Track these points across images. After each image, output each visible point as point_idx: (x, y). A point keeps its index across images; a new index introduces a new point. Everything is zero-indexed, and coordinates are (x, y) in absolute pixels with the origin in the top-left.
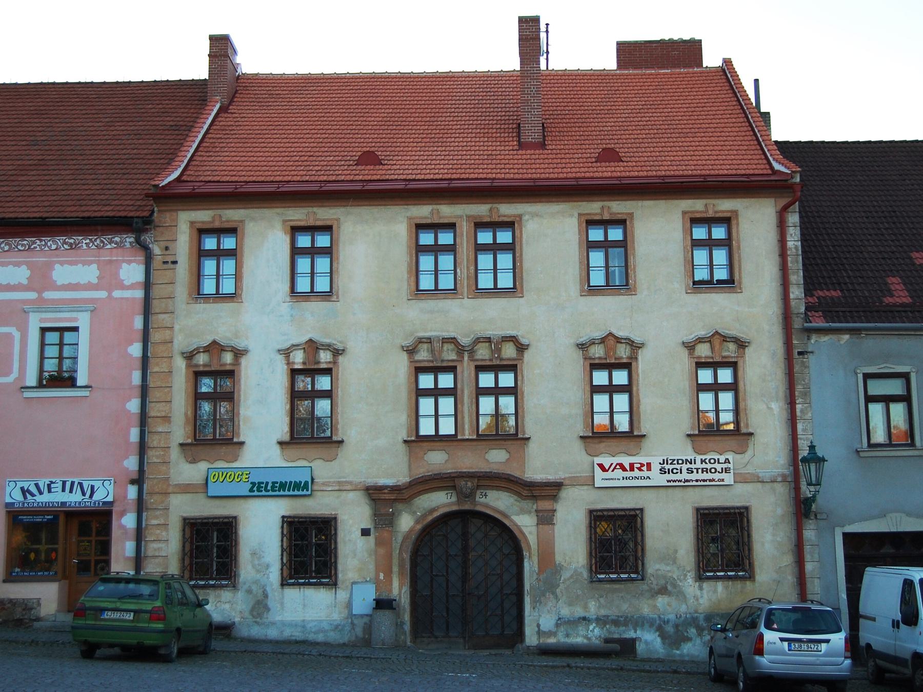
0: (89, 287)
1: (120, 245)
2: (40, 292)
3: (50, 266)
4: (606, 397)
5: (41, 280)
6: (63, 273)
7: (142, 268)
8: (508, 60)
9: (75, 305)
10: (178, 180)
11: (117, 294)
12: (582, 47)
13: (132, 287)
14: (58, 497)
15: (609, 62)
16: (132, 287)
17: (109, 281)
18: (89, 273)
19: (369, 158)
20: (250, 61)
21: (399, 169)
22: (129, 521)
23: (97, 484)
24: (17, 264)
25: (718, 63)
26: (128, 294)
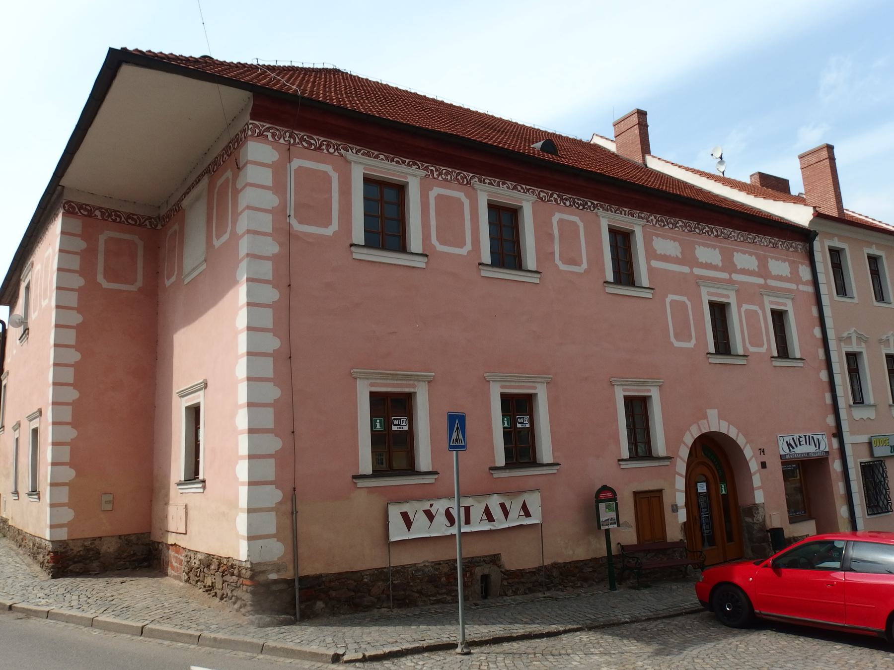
20: (254, 562)
23: (820, 437)
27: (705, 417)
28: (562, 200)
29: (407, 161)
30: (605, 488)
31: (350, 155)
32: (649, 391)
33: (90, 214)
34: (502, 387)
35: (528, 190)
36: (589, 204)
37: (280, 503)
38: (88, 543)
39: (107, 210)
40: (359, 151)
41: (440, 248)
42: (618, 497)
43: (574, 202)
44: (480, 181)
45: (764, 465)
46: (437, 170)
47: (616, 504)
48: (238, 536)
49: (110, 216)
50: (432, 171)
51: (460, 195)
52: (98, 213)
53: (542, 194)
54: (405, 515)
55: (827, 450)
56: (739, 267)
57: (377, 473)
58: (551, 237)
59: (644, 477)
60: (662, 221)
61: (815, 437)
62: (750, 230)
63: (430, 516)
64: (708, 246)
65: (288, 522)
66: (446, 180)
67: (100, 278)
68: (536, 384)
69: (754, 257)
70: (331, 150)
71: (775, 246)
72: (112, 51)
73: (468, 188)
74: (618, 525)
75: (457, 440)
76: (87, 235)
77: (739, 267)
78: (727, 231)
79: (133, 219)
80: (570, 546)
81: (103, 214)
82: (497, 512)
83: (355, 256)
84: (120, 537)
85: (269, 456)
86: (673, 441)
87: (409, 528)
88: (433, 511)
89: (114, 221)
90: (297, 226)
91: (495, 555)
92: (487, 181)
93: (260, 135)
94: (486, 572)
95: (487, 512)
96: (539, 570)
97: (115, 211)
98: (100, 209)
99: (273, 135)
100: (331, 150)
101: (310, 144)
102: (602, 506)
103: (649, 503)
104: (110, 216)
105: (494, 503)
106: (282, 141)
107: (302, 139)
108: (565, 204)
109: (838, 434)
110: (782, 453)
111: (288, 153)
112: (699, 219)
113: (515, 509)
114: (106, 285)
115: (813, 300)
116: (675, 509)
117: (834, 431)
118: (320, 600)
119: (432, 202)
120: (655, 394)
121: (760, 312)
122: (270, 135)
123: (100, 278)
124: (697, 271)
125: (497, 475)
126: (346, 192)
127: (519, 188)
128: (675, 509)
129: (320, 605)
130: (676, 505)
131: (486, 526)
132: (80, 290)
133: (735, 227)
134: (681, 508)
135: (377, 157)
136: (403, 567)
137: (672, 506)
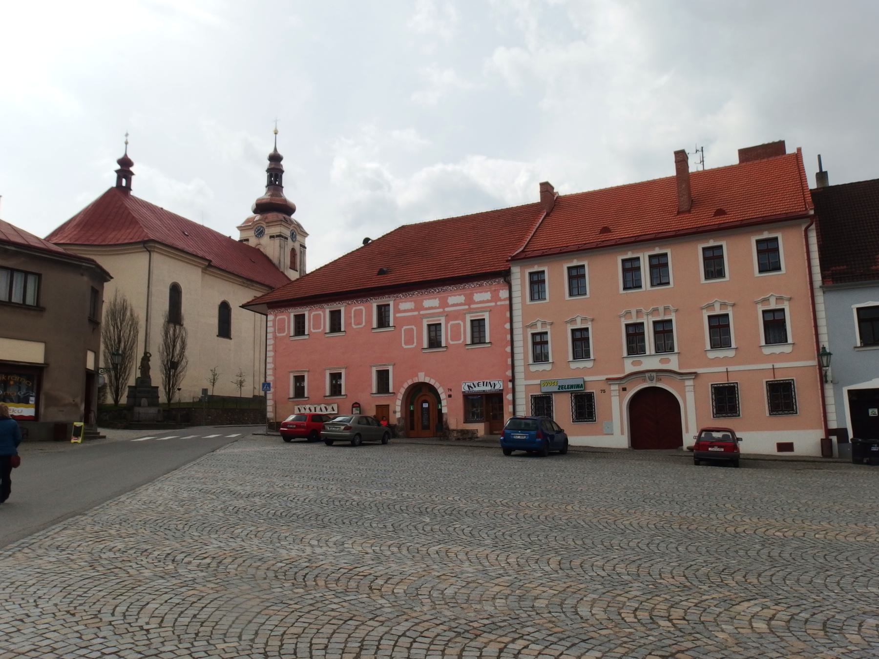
0: (488, 301)
1: (499, 283)
2: (469, 305)
3: (472, 295)
4: (14, 300)
5: (469, 301)
6: (477, 297)
7: (508, 292)
8: (671, 172)
9: (483, 310)
10: (523, 251)
11: (499, 303)
12: (722, 155)
13: (505, 300)
14: (482, 388)
15: (735, 160)
16: (505, 300)
17: (495, 298)
18: (487, 296)
19: (605, 230)
20: (563, 189)
21: (618, 234)
22: (509, 397)
23: (496, 382)
24: (460, 295)
25: (795, 151)
26: (503, 303)
27: (417, 376)
31: (291, 310)
45: (450, 396)
48: (496, 305)
51: (320, 312)
57: (473, 343)
59: (383, 400)
62: (461, 283)
82: (324, 409)
86: (397, 387)
87: (243, 306)
103: (383, 410)
105: (323, 406)
109: (513, 380)
111: (276, 316)
113: (330, 409)
116: (395, 412)
120: (390, 369)
124: (422, 312)
128: (395, 412)
133: (450, 285)
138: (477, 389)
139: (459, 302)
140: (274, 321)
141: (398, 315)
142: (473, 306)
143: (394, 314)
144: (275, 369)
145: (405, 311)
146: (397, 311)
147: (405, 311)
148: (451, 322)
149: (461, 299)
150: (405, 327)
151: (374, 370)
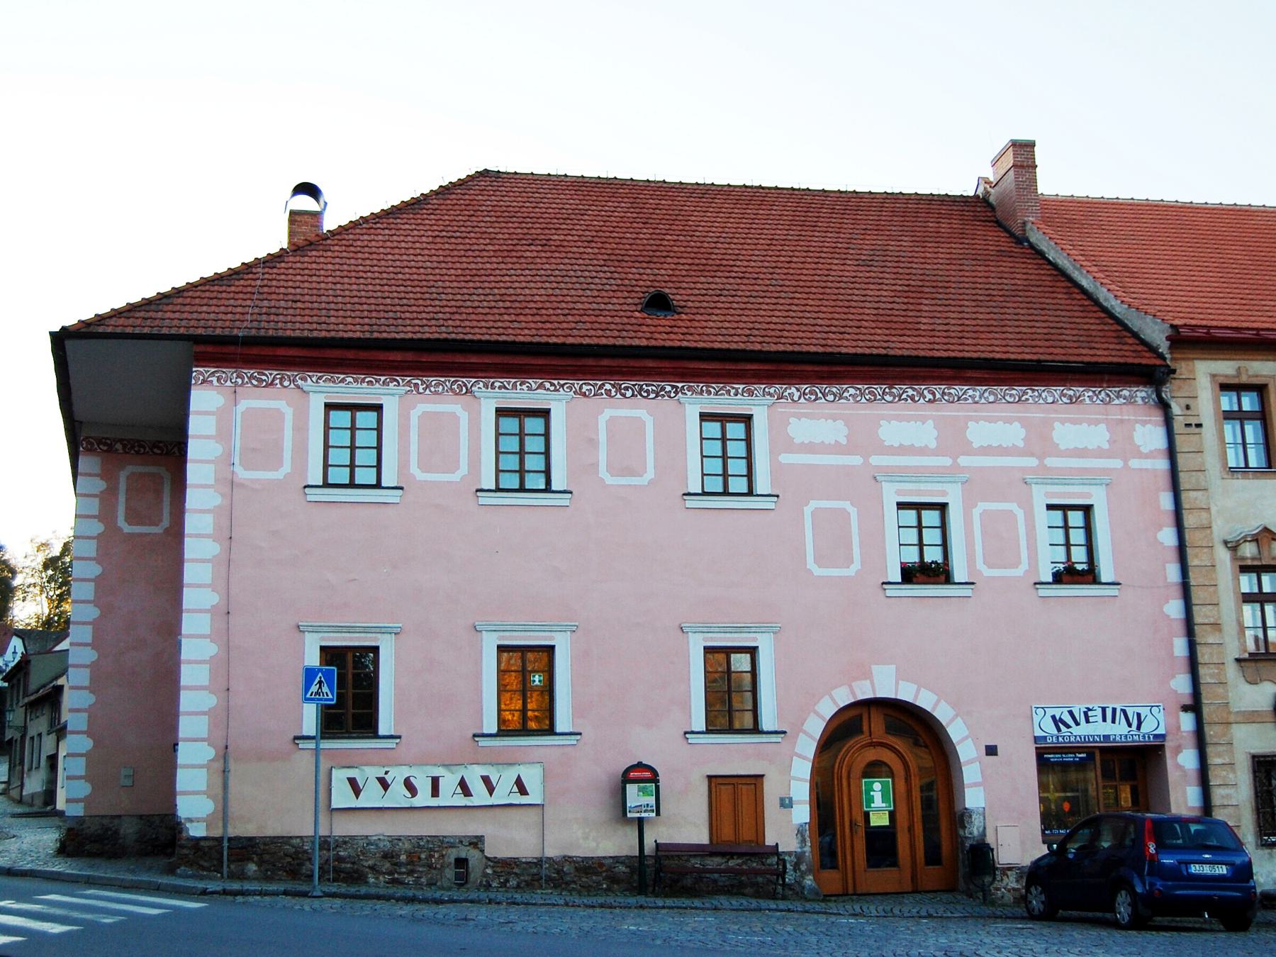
0: (1100, 453)
1: (1130, 401)
3: (1048, 424)
11: (1135, 463)
17: (1124, 447)
23: (1144, 712)
24: (1009, 421)
26: (1147, 464)
27: (868, 675)
28: (619, 390)
29: (383, 378)
30: (640, 766)
31: (308, 385)
32: (552, 638)
33: (110, 449)
34: (705, 640)
35: (562, 386)
36: (668, 388)
37: (212, 760)
38: (105, 821)
39: (129, 441)
40: (320, 378)
41: (420, 476)
42: (660, 778)
43: (641, 389)
44: (486, 386)
46: (423, 383)
47: (657, 788)
49: (133, 447)
50: (416, 385)
51: (281, 405)
52: (119, 446)
53: (585, 388)
54: (353, 782)
55: (1161, 731)
56: (975, 445)
58: (593, 443)
59: (733, 755)
60: (811, 393)
61: (1130, 712)
63: (384, 784)
64: (899, 418)
65: (218, 781)
66: (436, 393)
67: (121, 522)
68: (553, 634)
69: (1017, 424)
70: (286, 383)
71: (1073, 401)
72: (53, 335)
73: (468, 398)
74: (658, 813)
75: (317, 693)
76: (108, 475)
77: (975, 445)
78: (957, 390)
79: (159, 448)
80: (590, 837)
81: (124, 446)
83: (310, 498)
84: (141, 817)
85: (204, 713)
88: (389, 778)
89: (137, 453)
90: (242, 474)
91: (476, 837)
92: (497, 384)
93: (204, 381)
94: (463, 855)
95: (463, 784)
96: (539, 862)
97: (138, 441)
98: (121, 441)
99: (219, 379)
100: (286, 383)
101: (260, 381)
102: (632, 789)
103: (736, 795)
104: (133, 447)
106: (229, 383)
107: (252, 377)
108: (624, 395)
110: (1038, 733)
112: (914, 379)
114: (127, 529)
115: (1164, 481)
116: (786, 803)
117: (1188, 701)
118: (251, 860)
119: (414, 421)
120: (764, 643)
121: (1020, 514)
122: (214, 379)
123: (121, 522)
124: (875, 460)
125: (483, 742)
126: (301, 429)
127: (547, 385)
128: (786, 803)
129: (252, 867)
130: (791, 799)
131: (461, 801)
132: (98, 537)
134: (800, 802)
135: (343, 381)
136: (352, 838)
137: (782, 800)
138: (1083, 730)
139: (829, 440)
140: (223, 417)
141: (785, 458)
142: (1051, 462)
143: (774, 453)
144: (224, 613)
145: (810, 448)
146: (782, 443)
147: (810, 448)
148: (982, 506)
149: (1014, 434)
150: (853, 511)
151: (490, 643)
